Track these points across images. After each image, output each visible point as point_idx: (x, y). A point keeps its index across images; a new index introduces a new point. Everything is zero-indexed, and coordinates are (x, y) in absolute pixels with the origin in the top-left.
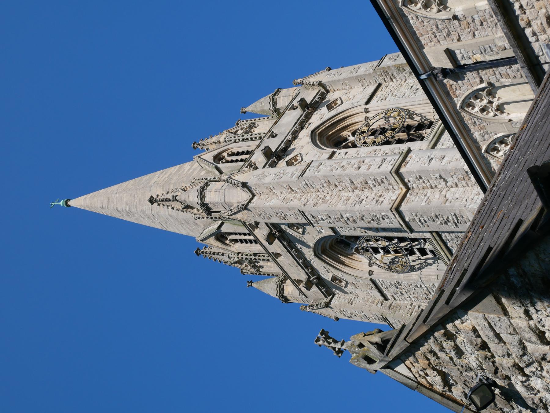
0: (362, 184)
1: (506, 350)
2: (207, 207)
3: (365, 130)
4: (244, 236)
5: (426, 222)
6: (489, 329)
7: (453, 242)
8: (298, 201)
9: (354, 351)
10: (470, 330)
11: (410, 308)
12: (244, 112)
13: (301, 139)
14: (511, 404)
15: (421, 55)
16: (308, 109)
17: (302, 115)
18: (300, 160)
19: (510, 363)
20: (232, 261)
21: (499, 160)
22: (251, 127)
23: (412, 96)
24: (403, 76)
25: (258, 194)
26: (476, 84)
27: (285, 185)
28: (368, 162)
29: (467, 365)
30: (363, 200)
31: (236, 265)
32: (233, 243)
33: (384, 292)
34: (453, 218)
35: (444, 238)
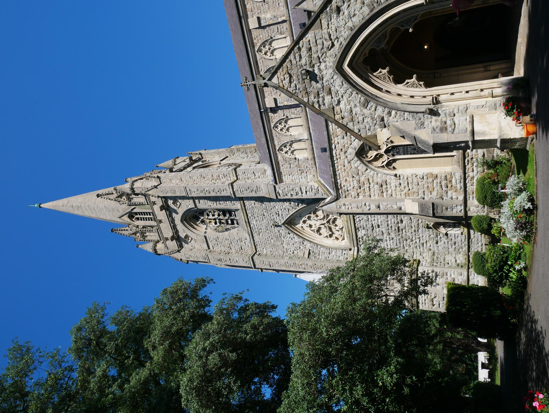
12: (157, 167)
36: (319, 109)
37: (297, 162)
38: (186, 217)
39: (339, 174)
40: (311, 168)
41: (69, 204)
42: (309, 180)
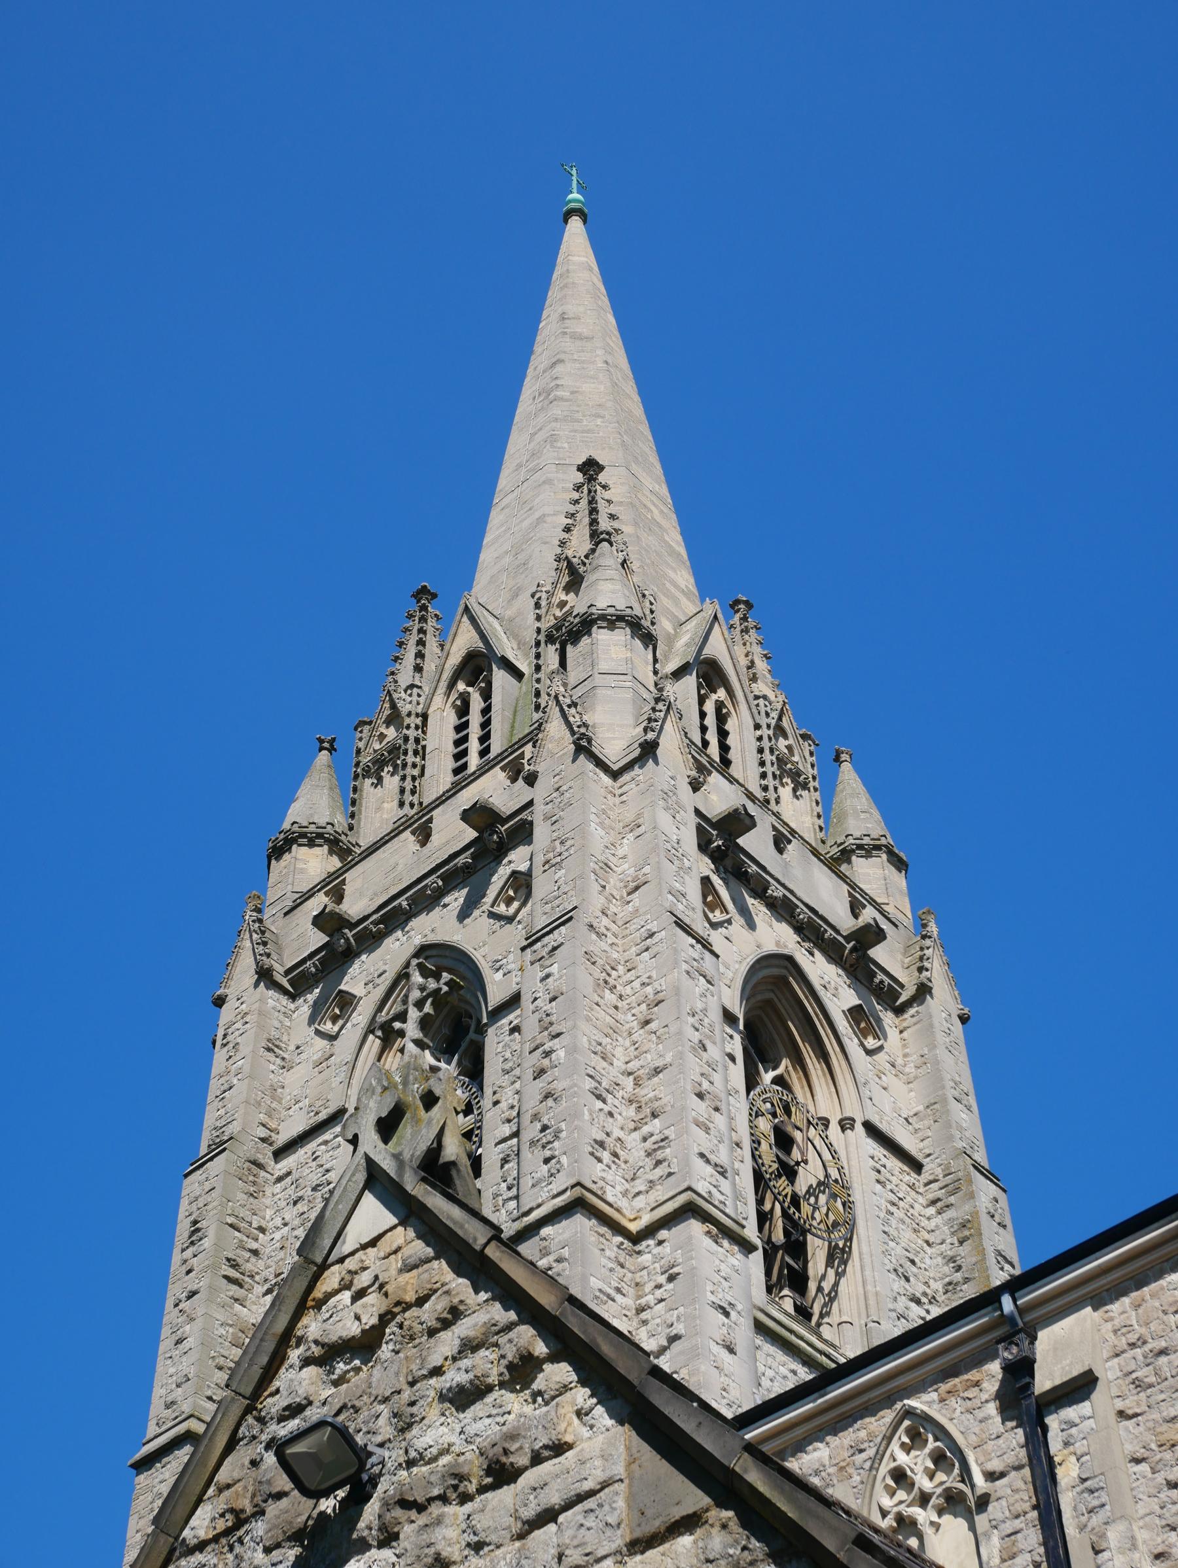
0: (651, 1100)
1: (493, 1538)
2: (579, 632)
3: (793, 1116)
4: (478, 736)
6: (573, 1493)
8: (599, 906)
9: (411, 1077)
10: (560, 1437)
11: (250, 1224)
12: (837, 759)
13: (771, 926)
14: (283, 1544)
15: (1076, 1299)
17: (837, 931)
18: (714, 920)
19: (449, 1549)
20: (401, 698)
22: (795, 775)
23: (887, 1261)
24: (943, 1237)
25: (621, 787)
26: (982, 1459)
27: (647, 869)
28: (716, 1122)
29: (417, 1419)
30: (604, 1101)
31: (387, 705)
32: (458, 703)
33: (301, 1147)
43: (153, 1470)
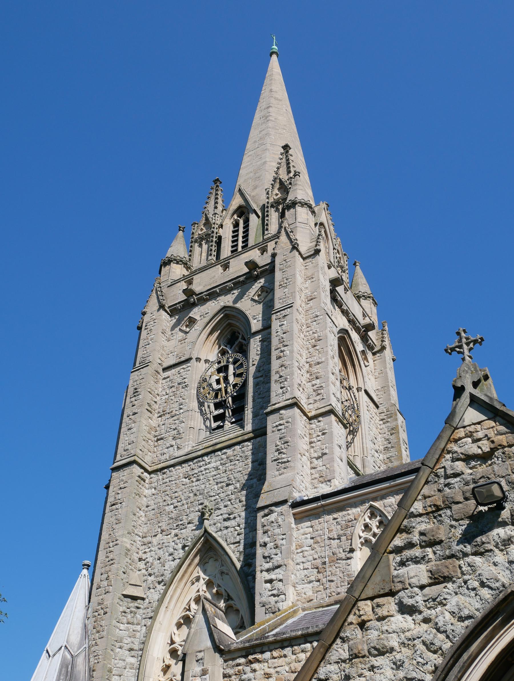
0: (316, 373)
2: (290, 206)
5: (279, 430)
7: (239, 452)
12: (355, 264)
16: (364, 331)
21: (361, 517)
25: (306, 263)
27: (316, 293)
31: (204, 219)
32: (234, 223)
33: (174, 369)
34: (284, 459)
35: (246, 443)
36: (390, 549)
37: (343, 555)
38: (234, 316)
39: (285, 656)
40: (328, 591)
41: (273, 101)
42: (299, 587)
43: (120, 472)
